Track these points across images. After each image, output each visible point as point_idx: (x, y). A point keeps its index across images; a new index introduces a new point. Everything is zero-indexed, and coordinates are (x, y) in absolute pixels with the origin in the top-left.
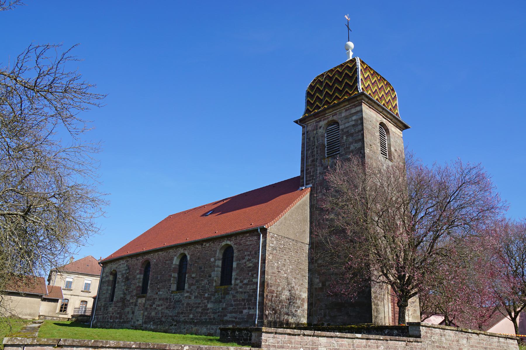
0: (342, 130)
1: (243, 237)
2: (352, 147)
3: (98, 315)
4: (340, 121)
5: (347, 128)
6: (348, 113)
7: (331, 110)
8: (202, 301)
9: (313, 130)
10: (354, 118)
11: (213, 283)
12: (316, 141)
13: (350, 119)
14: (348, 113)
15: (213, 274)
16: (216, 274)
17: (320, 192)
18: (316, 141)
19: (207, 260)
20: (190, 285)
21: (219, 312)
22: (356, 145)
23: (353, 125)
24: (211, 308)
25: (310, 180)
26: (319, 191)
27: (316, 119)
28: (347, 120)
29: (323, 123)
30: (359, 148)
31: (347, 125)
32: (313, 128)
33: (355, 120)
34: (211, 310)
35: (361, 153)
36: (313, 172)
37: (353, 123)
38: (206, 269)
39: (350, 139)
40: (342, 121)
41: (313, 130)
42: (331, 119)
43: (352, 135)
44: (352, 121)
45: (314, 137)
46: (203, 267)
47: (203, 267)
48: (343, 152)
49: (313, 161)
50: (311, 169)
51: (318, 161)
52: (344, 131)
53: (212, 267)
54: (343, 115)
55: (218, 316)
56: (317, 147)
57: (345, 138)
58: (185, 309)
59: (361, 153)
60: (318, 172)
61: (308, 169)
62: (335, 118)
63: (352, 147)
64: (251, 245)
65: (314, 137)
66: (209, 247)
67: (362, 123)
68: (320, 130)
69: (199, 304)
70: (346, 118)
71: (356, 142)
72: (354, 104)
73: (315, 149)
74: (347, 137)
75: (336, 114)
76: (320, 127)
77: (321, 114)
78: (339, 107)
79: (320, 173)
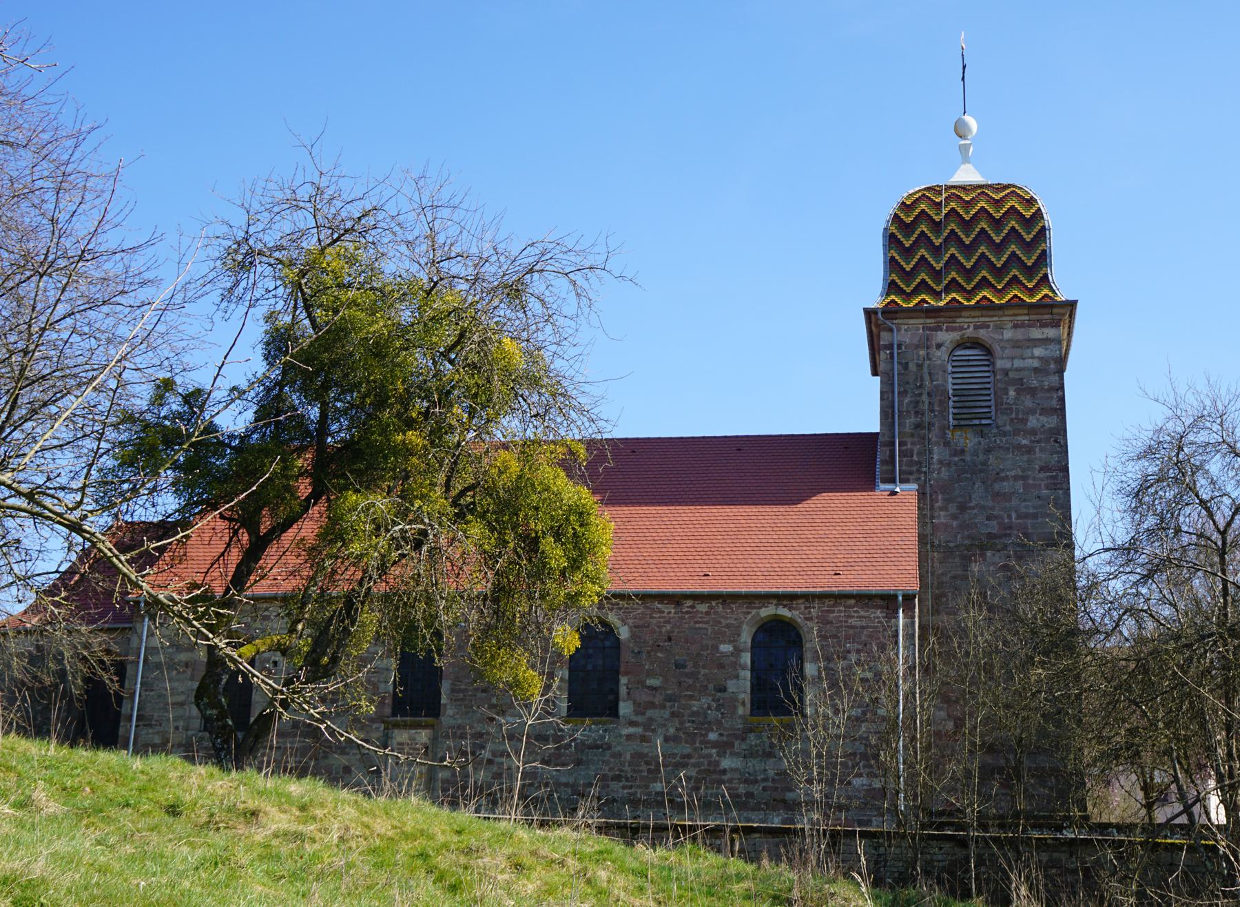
0: (1006, 372)
1: (833, 606)
2: (1033, 422)
3: (977, 842)
4: (996, 348)
5: (1017, 370)
6: (1019, 334)
7: (977, 313)
8: (695, 749)
9: (917, 347)
10: (1038, 352)
11: (735, 708)
12: (926, 377)
13: (1028, 353)
14: (1019, 334)
15: (731, 686)
16: (742, 686)
17: (941, 509)
18: (926, 377)
19: (704, 648)
20: (640, 709)
21: (765, 780)
22: (1044, 419)
23: (1036, 370)
24: (732, 770)
25: (911, 473)
26: (939, 504)
27: (929, 321)
28: (1018, 352)
29: (946, 337)
30: (1050, 429)
31: (1018, 363)
32: (915, 341)
33: (1040, 358)
34: (737, 776)
35: (1056, 441)
36: (919, 454)
37: (1036, 364)
38: (703, 671)
39: (1028, 402)
40: (1003, 348)
41: (917, 347)
42: (970, 332)
43: (1032, 391)
44: (1033, 357)
45: (920, 366)
46: (690, 664)
47: (690, 664)
48: (1008, 428)
49: (918, 426)
50: (913, 444)
51: (936, 429)
52: (1011, 375)
53: (728, 666)
54: (1008, 334)
55: (764, 789)
56: (929, 394)
57: (1012, 393)
58: (627, 768)
59: (1056, 441)
60: (936, 457)
61: (905, 444)
62: (982, 334)
63: (1033, 422)
64: (863, 627)
65: (920, 366)
66: (707, 613)
67: (1061, 371)
68: (939, 353)
69: (689, 756)
70: (1016, 344)
71: (1044, 411)
72: (1040, 317)
73: (925, 398)
74: (1018, 391)
75: (985, 326)
76: (939, 346)
77: (947, 314)
78: (1001, 313)
79: (940, 462)
